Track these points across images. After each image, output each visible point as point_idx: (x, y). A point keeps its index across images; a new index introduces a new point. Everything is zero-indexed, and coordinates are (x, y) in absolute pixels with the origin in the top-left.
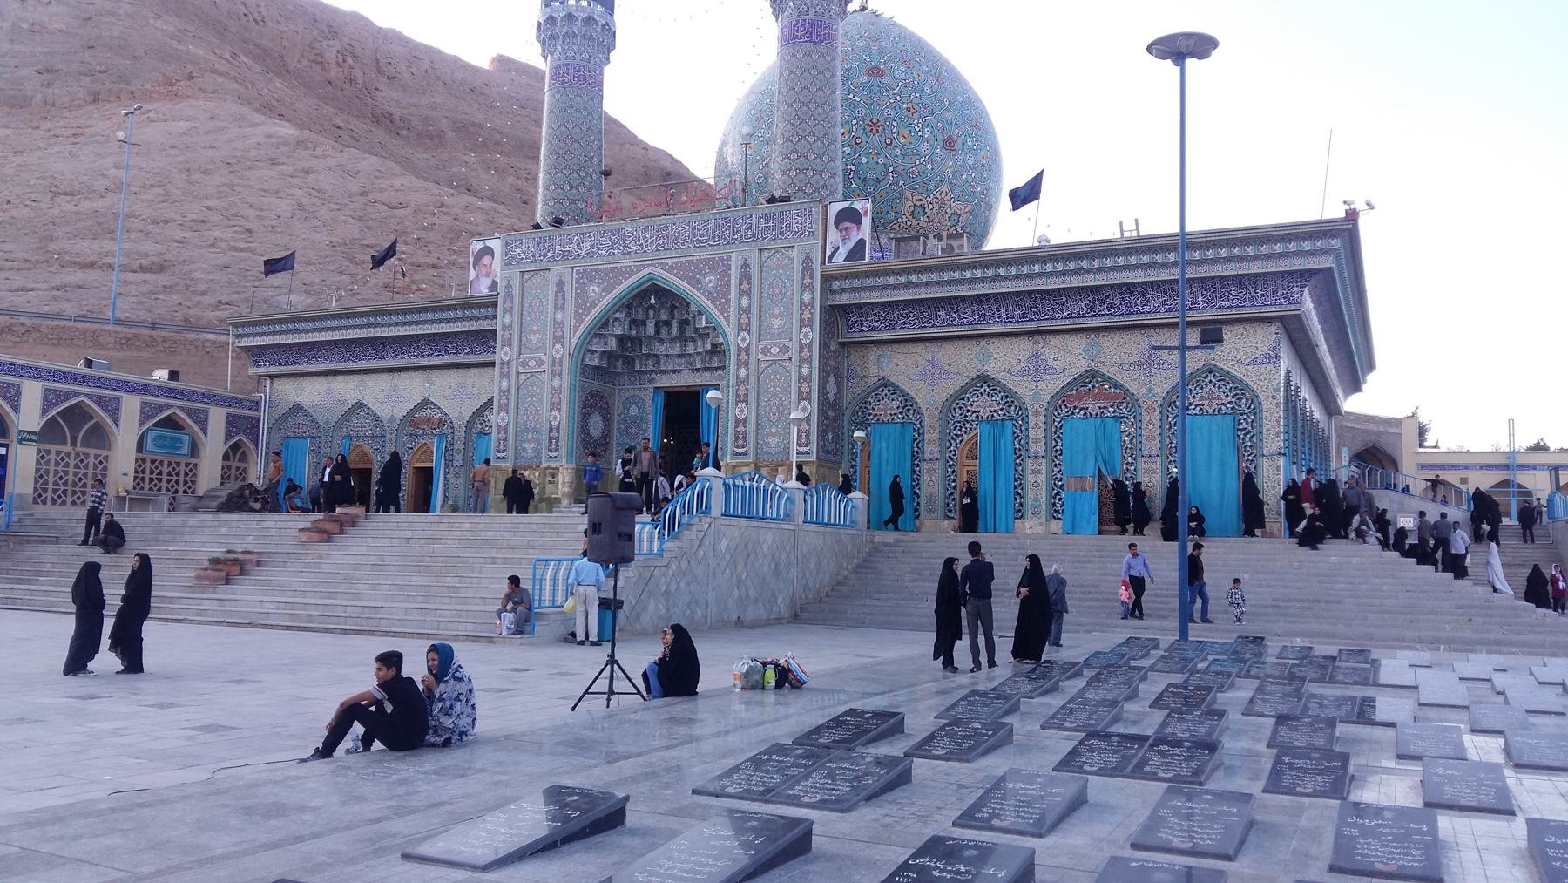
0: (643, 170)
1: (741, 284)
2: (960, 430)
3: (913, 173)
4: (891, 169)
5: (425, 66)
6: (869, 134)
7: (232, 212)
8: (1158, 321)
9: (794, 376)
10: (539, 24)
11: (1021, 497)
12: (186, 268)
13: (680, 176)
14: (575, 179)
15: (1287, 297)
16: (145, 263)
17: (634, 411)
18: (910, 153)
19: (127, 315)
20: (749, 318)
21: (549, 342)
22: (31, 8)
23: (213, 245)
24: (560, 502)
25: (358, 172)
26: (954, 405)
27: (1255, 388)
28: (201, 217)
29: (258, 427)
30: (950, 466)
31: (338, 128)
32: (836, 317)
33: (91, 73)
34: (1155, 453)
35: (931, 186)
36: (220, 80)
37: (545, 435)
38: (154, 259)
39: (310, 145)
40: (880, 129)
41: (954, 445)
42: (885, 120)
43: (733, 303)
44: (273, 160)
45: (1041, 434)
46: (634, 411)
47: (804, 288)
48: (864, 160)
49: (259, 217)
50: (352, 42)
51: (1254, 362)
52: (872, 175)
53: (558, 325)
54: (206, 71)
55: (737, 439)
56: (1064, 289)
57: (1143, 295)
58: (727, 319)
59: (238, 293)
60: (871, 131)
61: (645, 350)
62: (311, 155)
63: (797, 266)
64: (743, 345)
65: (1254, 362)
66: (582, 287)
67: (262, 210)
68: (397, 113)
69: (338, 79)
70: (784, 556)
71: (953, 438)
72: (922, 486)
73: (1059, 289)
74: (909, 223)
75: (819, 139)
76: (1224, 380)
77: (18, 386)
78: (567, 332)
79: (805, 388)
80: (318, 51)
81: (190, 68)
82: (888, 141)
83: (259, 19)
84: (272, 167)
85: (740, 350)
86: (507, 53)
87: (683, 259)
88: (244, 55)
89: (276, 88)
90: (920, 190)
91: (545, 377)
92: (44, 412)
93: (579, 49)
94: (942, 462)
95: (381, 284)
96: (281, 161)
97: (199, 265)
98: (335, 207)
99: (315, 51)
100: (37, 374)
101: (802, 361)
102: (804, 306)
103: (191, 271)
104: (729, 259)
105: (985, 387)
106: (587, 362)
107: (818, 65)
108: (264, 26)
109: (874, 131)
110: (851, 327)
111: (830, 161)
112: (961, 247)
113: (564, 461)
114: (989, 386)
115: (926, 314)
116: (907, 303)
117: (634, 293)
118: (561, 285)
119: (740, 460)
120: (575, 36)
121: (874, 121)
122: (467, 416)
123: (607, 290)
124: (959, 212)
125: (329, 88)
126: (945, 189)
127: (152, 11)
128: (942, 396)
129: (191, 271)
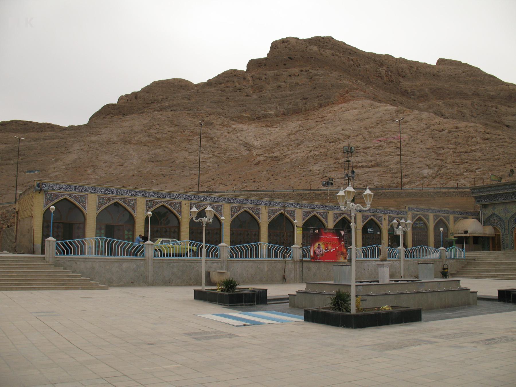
0: (508, 94)
5: (415, 69)
23: (390, 155)
33: (317, 97)
54: (352, 89)
59: (408, 171)
69: (387, 81)
77: (180, 203)
81: (347, 89)
84: (393, 122)
86: (441, 58)
95: (452, 162)
99: (378, 73)
100: (432, 211)
108: (360, 67)
125: (385, 85)
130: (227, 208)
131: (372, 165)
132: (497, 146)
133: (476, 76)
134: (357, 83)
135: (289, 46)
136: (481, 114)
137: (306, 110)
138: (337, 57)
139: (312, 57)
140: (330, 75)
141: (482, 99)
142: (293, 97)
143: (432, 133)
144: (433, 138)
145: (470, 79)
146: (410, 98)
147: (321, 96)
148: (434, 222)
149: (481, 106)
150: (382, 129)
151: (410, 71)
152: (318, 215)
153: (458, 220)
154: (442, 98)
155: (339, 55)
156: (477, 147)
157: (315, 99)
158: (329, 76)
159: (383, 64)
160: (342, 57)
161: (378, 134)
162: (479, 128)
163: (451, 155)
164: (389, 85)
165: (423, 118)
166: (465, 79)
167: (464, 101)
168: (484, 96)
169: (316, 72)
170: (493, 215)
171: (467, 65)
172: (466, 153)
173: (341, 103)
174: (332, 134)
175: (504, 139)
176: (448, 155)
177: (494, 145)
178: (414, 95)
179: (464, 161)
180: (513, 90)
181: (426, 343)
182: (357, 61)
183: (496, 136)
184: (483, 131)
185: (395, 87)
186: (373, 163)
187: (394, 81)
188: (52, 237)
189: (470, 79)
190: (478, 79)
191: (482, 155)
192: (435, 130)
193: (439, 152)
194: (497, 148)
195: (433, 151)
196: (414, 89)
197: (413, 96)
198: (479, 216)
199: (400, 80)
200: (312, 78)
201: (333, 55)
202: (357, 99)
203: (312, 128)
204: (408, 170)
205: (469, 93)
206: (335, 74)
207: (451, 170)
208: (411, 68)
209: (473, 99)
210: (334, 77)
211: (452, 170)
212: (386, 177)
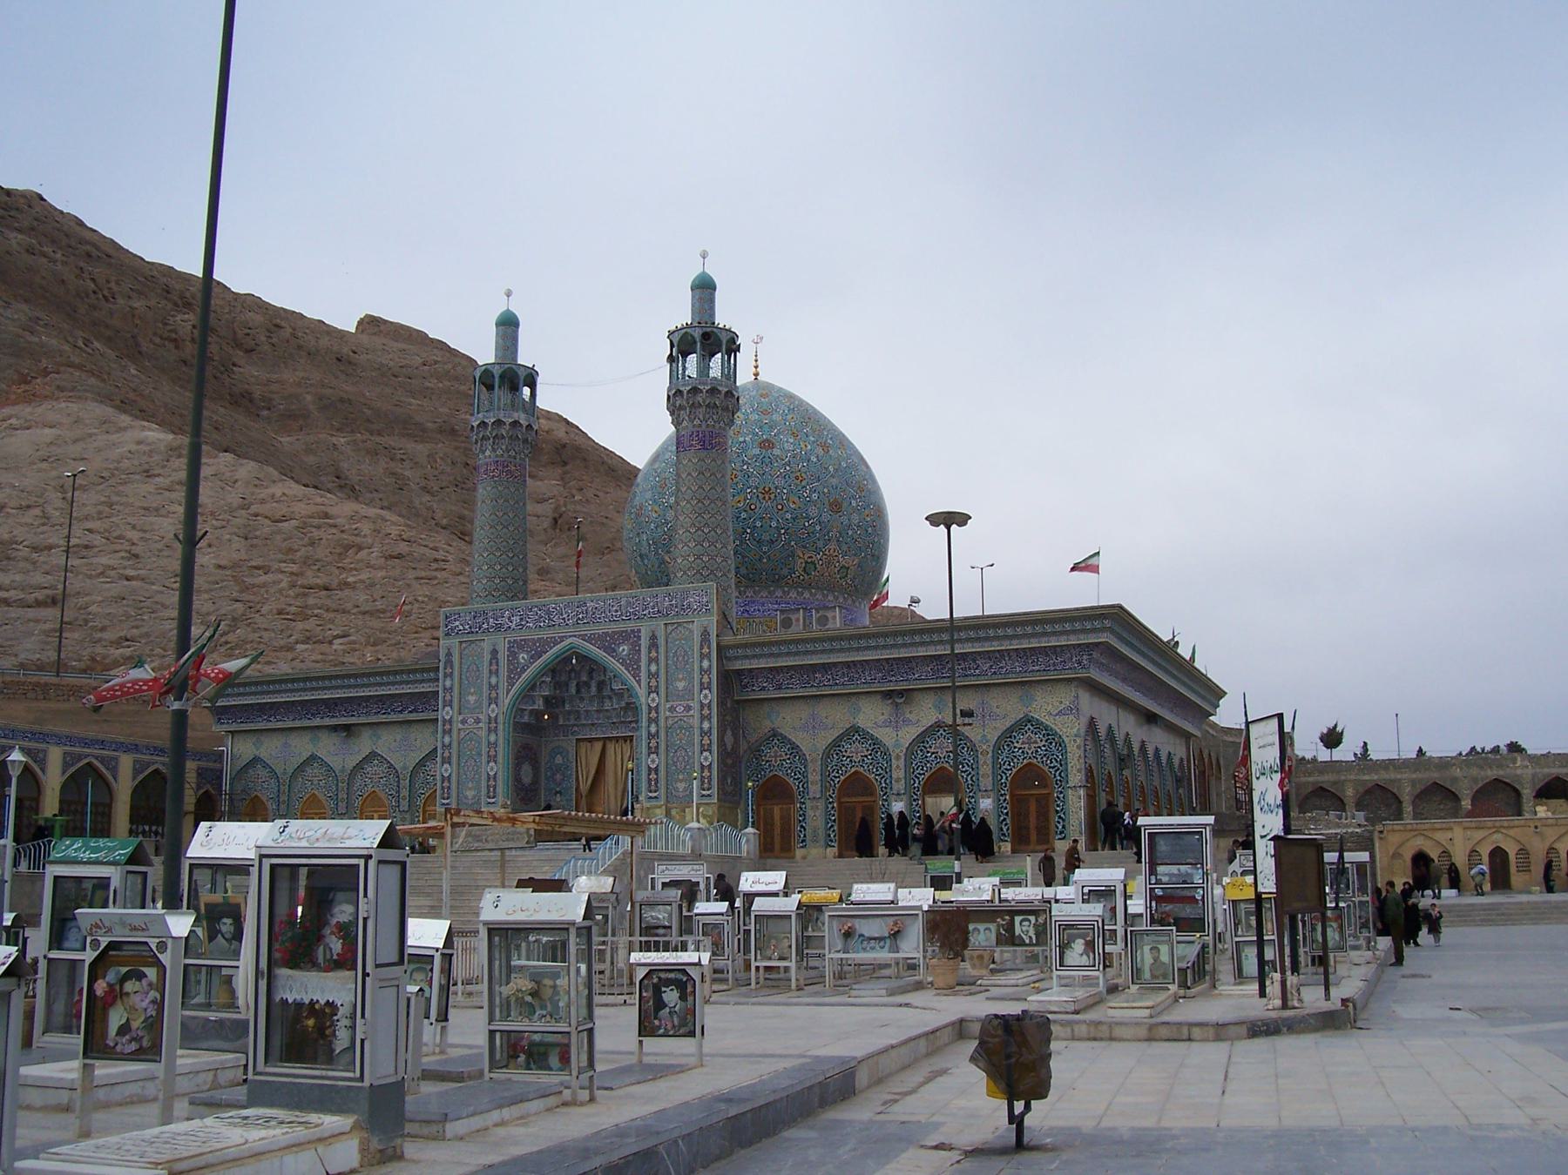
3: (804, 533)
4: (783, 531)
7: (115, 534)
9: (697, 732)
11: (1064, 820)
12: (82, 601)
13: (578, 449)
14: (504, 560)
15: (1079, 663)
17: (559, 760)
21: (485, 703)
30: (1002, 795)
32: (730, 681)
34: (990, 788)
35: (820, 544)
37: (484, 783)
40: (772, 496)
42: (776, 488)
43: (643, 669)
44: (147, 471)
45: (902, 774)
46: (559, 760)
47: (702, 656)
48: (758, 524)
52: (766, 537)
55: (650, 785)
57: (974, 661)
58: (639, 682)
59: (137, 627)
60: (764, 498)
61: (567, 707)
63: (697, 638)
66: (513, 655)
67: (145, 531)
68: (257, 392)
73: (909, 657)
78: (501, 695)
79: (706, 741)
81: (44, 363)
82: (780, 507)
90: (811, 548)
91: (483, 733)
92: (134, 778)
94: (823, 800)
95: (275, 611)
96: (156, 472)
97: (94, 597)
99: (169, 328)
100: (60, 740)
101: (703, 718)
104: (639, 631)
118: (494, 652)
119: (654, 803)
120: (503, 437)
121: (767, 489)
130: (55, 755)
131: (36, 600)
132: (417, 578)
133: (457, 378)
136: (453, 488)
138: (44, 260)
143: (251, 523)
144: (246, 539)
146: (258, 415)
148: (64, 773)
150: (109, 497)
152: (96, 762)
154: (349, 429)
156: (364, 576)
159: (190, 304)
160: (58, 264)
161: (90, 510)
162: (388, 523)
163: (280, 591)
167: (410, 446)
170: (256, 760)
172: (327, 589)
173: (14, 403)
175: (443, 561)
176: (272, 591)
177: (411, 574)
178: (269, 409)
179: (310, 612)
180: (547, 432)
182: (108, 282)
183: (423, 550)
184: (397, 532)
185: (215, 377)
186: (40, 595)
191: (367, 601)
192: (261, 515)
193: (249, 580)
194: (415, 584)
195: (233, 576)
196: (271, 392)
197: (265, 413)
198: (221, 762)
201: (30, 251)
202: (70, 397)
204: (140, 623)
207: (263, 633)
208: (276, 329)
210: (13, 320)
211: (266, 635)
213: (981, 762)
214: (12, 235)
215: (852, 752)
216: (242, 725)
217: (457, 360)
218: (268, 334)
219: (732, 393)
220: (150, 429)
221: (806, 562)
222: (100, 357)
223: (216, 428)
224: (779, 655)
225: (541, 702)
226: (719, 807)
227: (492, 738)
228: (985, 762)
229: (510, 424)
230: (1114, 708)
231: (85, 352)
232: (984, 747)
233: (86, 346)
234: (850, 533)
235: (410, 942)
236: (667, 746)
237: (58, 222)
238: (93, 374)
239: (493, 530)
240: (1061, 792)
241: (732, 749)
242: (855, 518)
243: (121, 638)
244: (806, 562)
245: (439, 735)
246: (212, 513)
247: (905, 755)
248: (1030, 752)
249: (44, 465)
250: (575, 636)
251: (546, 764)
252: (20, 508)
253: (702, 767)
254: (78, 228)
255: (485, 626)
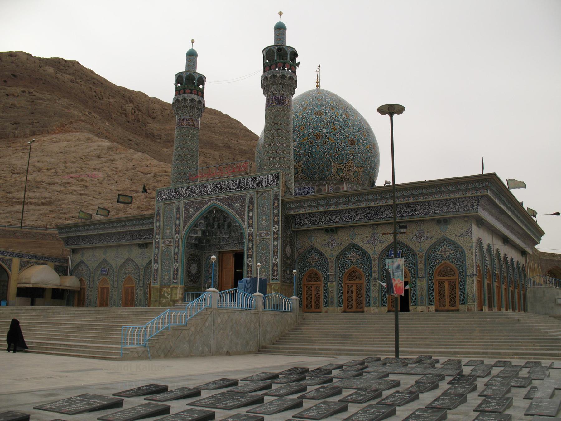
1: (249, 207)
2: (344, 268)
4: (326, 154)
6: (316, 139)
7: (80, 179)
8: (414, 219)
9: (271, 246)
10: (262, 80)
11: (464, 294)
15: (472, 207)
16: (44, 201)
18: (334, 147)
19: (33, 223)
20: (253, 221)
21: (174, 233)
22: (11, 99)
23: (71, 193)
24: (178, 301)
25: (133, 159)
26: (341, 257)
27: (462, 246)
28: (68, 181)
29: (67, 270)
30: (340, 284)
31: (130, 140)
35: (344, 160)
36: (83, 124)
38: (48, 199)
39: (114, 149)
40: (321, 137)
41: (341, 274)
43: (246, 215)
45: (376, 269)
47: (275, 208)
48: (314, 150)
49: (92, 181)
50: (138, 105)
51: (462, 235)
52: (318, 156)
53: (177, 226)
55: (274, 272)
56: (382, 206)
57: (415, 207)
58: (244, 222)
60: (317, 138)
62: (115, 153)
63: (272, 198)
64: (250, 233)
65: (462, 235)
66: (186, 210)
68: (156, 133)
70: (253, 325)
71: (341, 272)
72: (328, 293)
73: (380, 206)
74: (335, 176)
75: (282, 144)
76: (450, 243)
78: (181, 230)
80: (124, 109)
81: (71, 119)
83: (101, 97)
85: (249, 235)
87: (226, 197)
88: (94, 112)
89: (106, 125)
93: (188, 112)
95: (136, 207)
96: (102, 156)
97: (65, 201)
98: (121, 175)
99: (123, 109)
101: (274, 239)
102: (275, 215)
103: (61, 204)
104: (245, 196)
105: (354, 249)
106: (189, 241)
107: (281, 114)
108: (103, 100)
109: (318, 138)
110: (297, 224)
111: (287, 153)
112: (343, 188)
113: (179, 284)
114: (355, 248)
115: (327, 217)
116: (319, 213)
117: (207, 211)
118: (178, 209)
120: (187, 106)
122: (145, 264)
123: (196, 211)
124: (358, 171)
125: (128, 124)
126: (351, 161)
127: (58, 97)
128: (336, 253)
129: (61, 204)
134: (89, 116)
135: (17, 62)
137: (14, 137)
138: (77, 85)
139: (42, 79)
140: (57, 101)
141: (233, 152)
142: (2, 120)
144: (131, 180)
145: (226, 130)
146: (156, 141)
147: (36, 123)
149: (229, 159)
151: (161, 113)
153: (27, 266)
155: (80, 82)
157: (28, 125)
158: (56, 102)
159: (132, 101)
161: (73, 170)
164: (133, 124)
165: (133, 158)
166: (220, 130)
167: (213, 152)
168: (235, 149)
169: (40, 96)
170: (81, 262)
171: (227, 117)
174: (22, 165)
178: (160, 139)
181: (14, 412)
182: (101, 92)
185: (140, 127)
187: (141, 120)
188: (214, 287)
189: (226, 130)
190: (233, 131)
196: (161, 133)
198: (67, 263)
199: (148, 121)
200: (33, 102)
201: (72, 81)
203: (6, 156)
205: (221, 145)
206: (65, 102)
209: (223, 151)
212: (48, 217)
213: (419, 262)
214: (65, 75)
215: (351, 257)
216: (76, 246)
217: (232, 121)
218: (161, 112)
219: (292, 78)
220: (104, 142)
221: (337, 169)
222: (94, 119)
223: (137, 145)
224: (313, 206)
225: (200, 233)
226: (282, 285)
227: (176, 250)
228: (421, 262)
229: (190, 100)
230: (491, 237)
231: (88, 116)
232: (421, 254)
233: (89, 114)
234: (359, 155)
235: (394, 315)
236: (257, 254)
237: (84, 71)
238: (89, 124)
239: (181, 150)
240: (463, 278)
241: (291, 255)
242: (362, 148)
243: (70, 217)
244: (337, 169)
245: (153, 250)
246: (120, 171)
247: (379, 258)
248: (445, 257)
249: (60, 154)
250: (215, 199)
251: (205, 264)
252: (48, 169)
253: (274, 264)
254: (92, 74)
255: (175, 196)
